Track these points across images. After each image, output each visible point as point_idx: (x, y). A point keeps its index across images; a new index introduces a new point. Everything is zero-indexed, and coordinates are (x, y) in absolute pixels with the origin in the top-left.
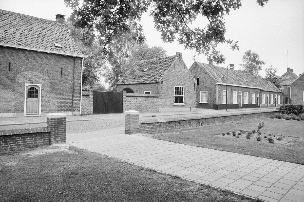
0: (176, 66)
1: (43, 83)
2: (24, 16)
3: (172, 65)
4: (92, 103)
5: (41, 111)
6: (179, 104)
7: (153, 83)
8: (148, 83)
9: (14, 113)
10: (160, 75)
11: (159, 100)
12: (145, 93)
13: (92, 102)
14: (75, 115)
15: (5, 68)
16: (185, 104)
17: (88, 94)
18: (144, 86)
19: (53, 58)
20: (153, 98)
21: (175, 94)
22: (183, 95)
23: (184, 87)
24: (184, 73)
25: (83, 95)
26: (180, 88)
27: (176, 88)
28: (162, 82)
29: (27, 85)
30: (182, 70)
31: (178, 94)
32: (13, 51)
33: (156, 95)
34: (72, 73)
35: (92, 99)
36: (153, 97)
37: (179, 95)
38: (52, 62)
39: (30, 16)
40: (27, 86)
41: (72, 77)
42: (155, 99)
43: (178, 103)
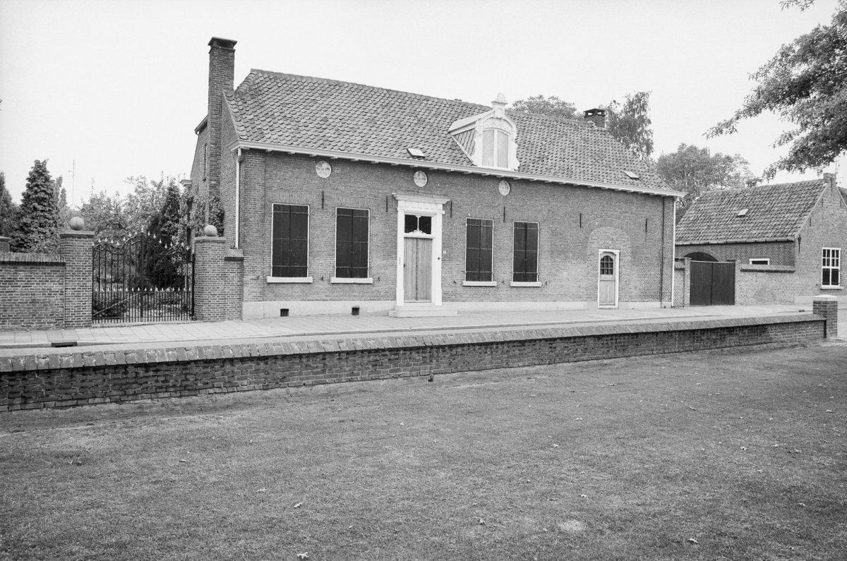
0: (825, 204)
1: (622, 247)
2: (315, 81)
3: (818, 201)
4: (689, 285)
5: (619, 299)
6: (831, 286)
7: (776, 242)
8: (763, 242)
9: (585, 303)
10: (794, 226)
11: (795, 277)
12: (751, 263)
13: (688, 283)
14: (665, 307)
15: (576, 222)
16: (842, 288)
17: (683, 267)
18: (749, 248)
19: (635, 200)
20: (784, 274)
21: (824, 265)
22: (839, 268)
23: (839, 249)
24: (840, 218)
25: (676, 269)
26: (833, 251)
27: (824, 251)
28: (799, 239)
29: (601, 251)
30: (837, 211)
31: (828, 265)
32: (443, 178)
33: (788, 268)
34: (661, 228)
35: (689, 277)
36: (785, 272)
37: (831, 267)
38: (634, 209)
39: (317, 78)
40: (601, 253)
41: (660, 236)
42: (788, 275)
43: (829, 284)
